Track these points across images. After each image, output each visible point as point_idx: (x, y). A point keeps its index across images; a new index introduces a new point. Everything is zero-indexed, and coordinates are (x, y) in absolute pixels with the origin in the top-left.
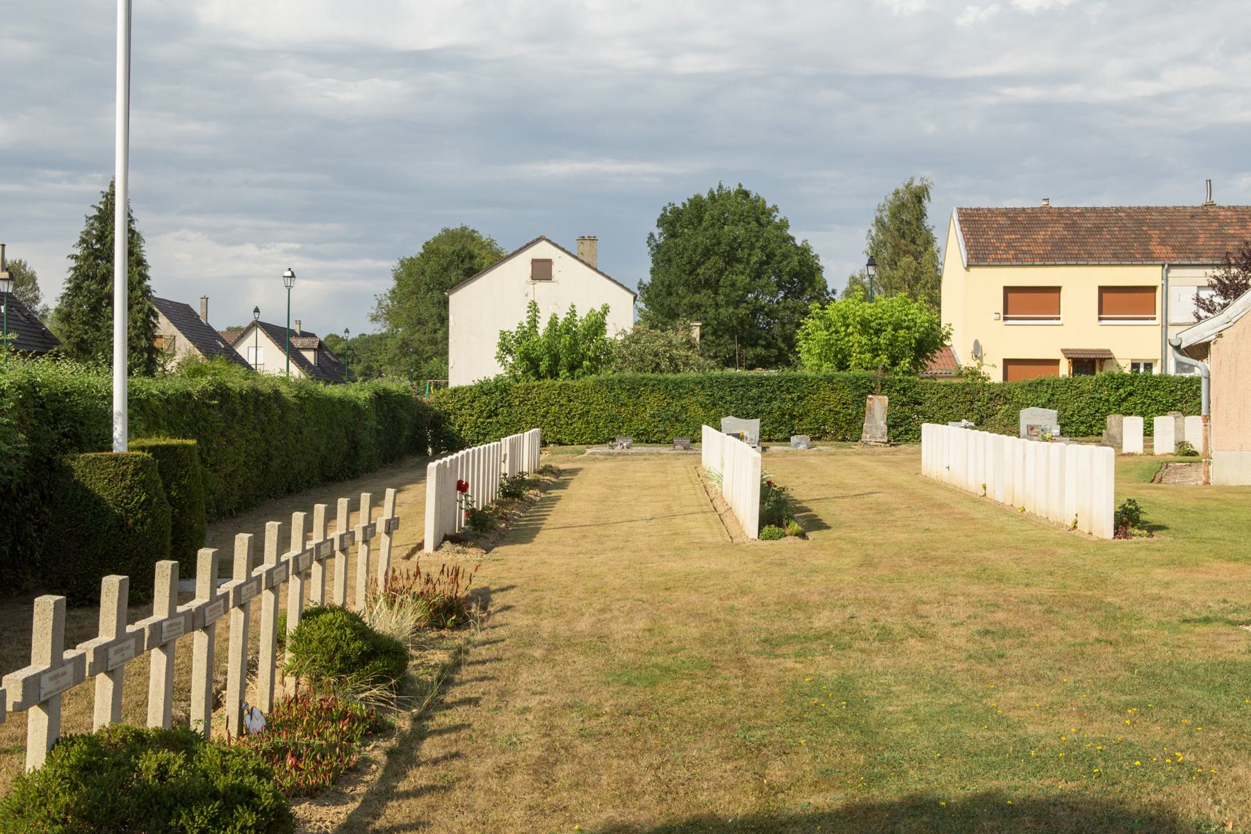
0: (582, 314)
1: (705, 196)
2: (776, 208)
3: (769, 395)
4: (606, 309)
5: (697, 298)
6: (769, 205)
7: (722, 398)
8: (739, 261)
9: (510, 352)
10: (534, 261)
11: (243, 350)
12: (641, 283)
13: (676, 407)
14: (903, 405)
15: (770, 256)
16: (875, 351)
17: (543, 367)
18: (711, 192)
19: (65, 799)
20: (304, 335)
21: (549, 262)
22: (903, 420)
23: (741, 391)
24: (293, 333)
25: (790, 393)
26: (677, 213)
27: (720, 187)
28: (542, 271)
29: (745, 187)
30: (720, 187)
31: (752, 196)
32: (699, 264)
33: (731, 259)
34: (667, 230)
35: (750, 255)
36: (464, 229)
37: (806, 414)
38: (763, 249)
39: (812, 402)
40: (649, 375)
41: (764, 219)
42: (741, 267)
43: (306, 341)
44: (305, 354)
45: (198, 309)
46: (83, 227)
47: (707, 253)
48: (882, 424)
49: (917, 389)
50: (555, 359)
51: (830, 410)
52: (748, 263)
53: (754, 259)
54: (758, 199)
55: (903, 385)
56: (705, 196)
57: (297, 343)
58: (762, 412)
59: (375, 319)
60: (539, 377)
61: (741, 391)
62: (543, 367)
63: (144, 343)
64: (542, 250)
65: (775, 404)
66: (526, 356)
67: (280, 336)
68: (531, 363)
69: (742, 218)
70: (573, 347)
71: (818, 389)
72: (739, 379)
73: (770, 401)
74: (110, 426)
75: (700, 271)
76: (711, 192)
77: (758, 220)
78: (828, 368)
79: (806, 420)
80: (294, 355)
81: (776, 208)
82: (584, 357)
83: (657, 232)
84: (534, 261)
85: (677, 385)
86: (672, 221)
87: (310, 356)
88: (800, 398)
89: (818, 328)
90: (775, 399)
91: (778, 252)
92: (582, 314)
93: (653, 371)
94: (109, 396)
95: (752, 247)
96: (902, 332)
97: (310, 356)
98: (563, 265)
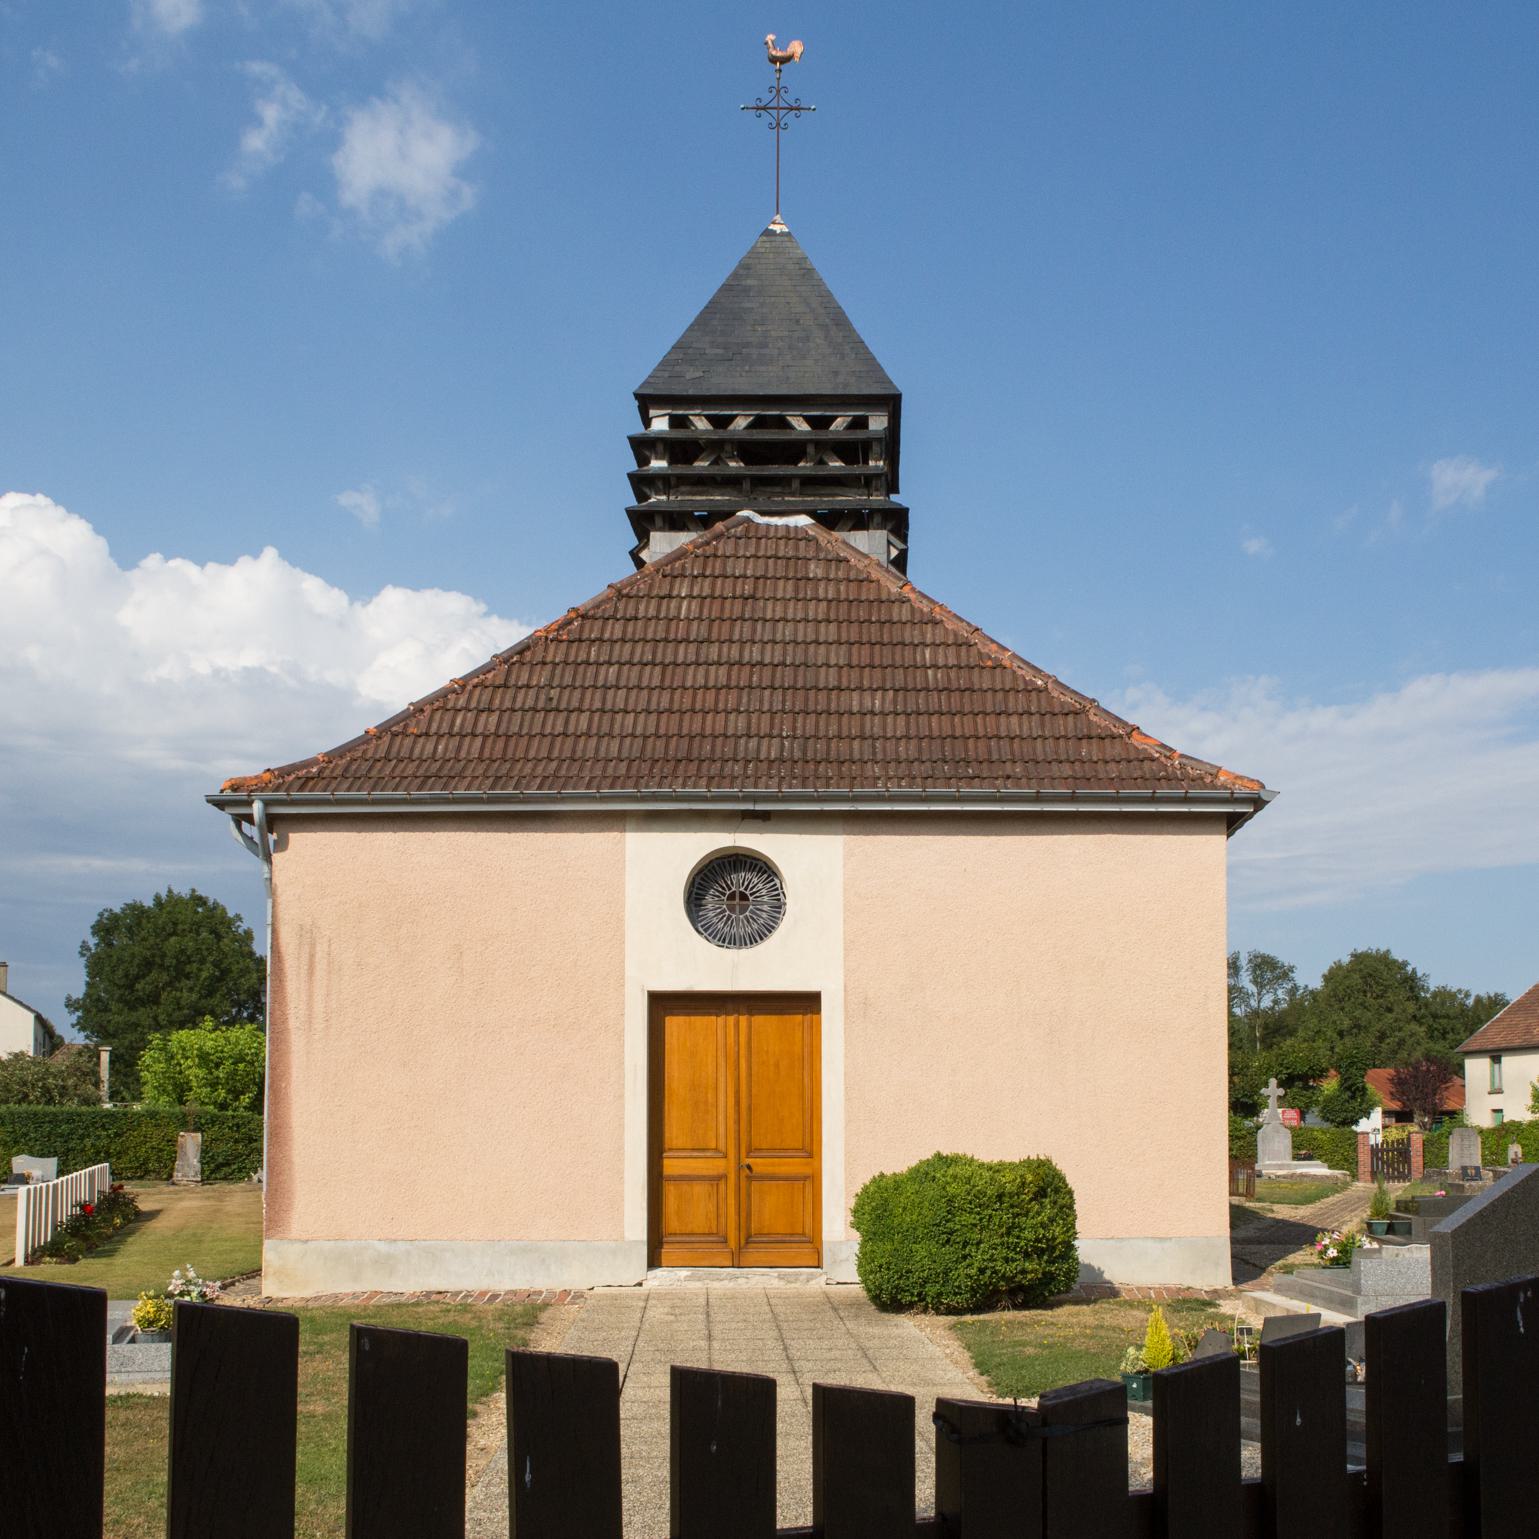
1: (149, 903)
2: (239, 918)
3: (81, 1132)
5: (134, 1017)
6: (231, 914)
7: (25, 1135)
8: (188, 977)
12: (69, 999)
14: (236, 1141)
15: (225, 972)
16: (214, 1085)
18: (157, 898)
19: (1428, 996)
22: (237, 1157)
23: (47, 1128)
25: (106, 1130)
26: (115, 919)
27: (170, 891)
29: (200, 892)
30: (170, 891)
31: (211, 902)
32: (137, 978)
33: (180, 974)
34: (102, 939)
35: (200, 970)
36: (1358, 958)
38: (216, 965)
41: (222, 930)
42: (190, 983)
47: (148, 965)
48: (194, 1161)
49: (252, 1126)
51: (153, 1148)
52: (198, 977)
53: (204, 974)
54: (216, 906)
55: (236, 1121)
56: (149, 903)
58: (73, 1149)
59: (1414, 969)
61: (47, 1128)
65: (88, 1142)
69: (196, 928)
71: (139, 1125)
72: (46, 1115)
73: (82, 1138)
75: (138, 986)
76: (157, 898)
77: (213, 931)
78: (163, 1104)
79: (125, 1159)
81: (239, 918)
83: (92, 941)
86: (107, 927)
88: (117, 1135)
89: (157, 1061)
90: (89, 1136)
91: (234, 968)
93: (19, 1102)
95: (203, 961)
96: (241, 1066)
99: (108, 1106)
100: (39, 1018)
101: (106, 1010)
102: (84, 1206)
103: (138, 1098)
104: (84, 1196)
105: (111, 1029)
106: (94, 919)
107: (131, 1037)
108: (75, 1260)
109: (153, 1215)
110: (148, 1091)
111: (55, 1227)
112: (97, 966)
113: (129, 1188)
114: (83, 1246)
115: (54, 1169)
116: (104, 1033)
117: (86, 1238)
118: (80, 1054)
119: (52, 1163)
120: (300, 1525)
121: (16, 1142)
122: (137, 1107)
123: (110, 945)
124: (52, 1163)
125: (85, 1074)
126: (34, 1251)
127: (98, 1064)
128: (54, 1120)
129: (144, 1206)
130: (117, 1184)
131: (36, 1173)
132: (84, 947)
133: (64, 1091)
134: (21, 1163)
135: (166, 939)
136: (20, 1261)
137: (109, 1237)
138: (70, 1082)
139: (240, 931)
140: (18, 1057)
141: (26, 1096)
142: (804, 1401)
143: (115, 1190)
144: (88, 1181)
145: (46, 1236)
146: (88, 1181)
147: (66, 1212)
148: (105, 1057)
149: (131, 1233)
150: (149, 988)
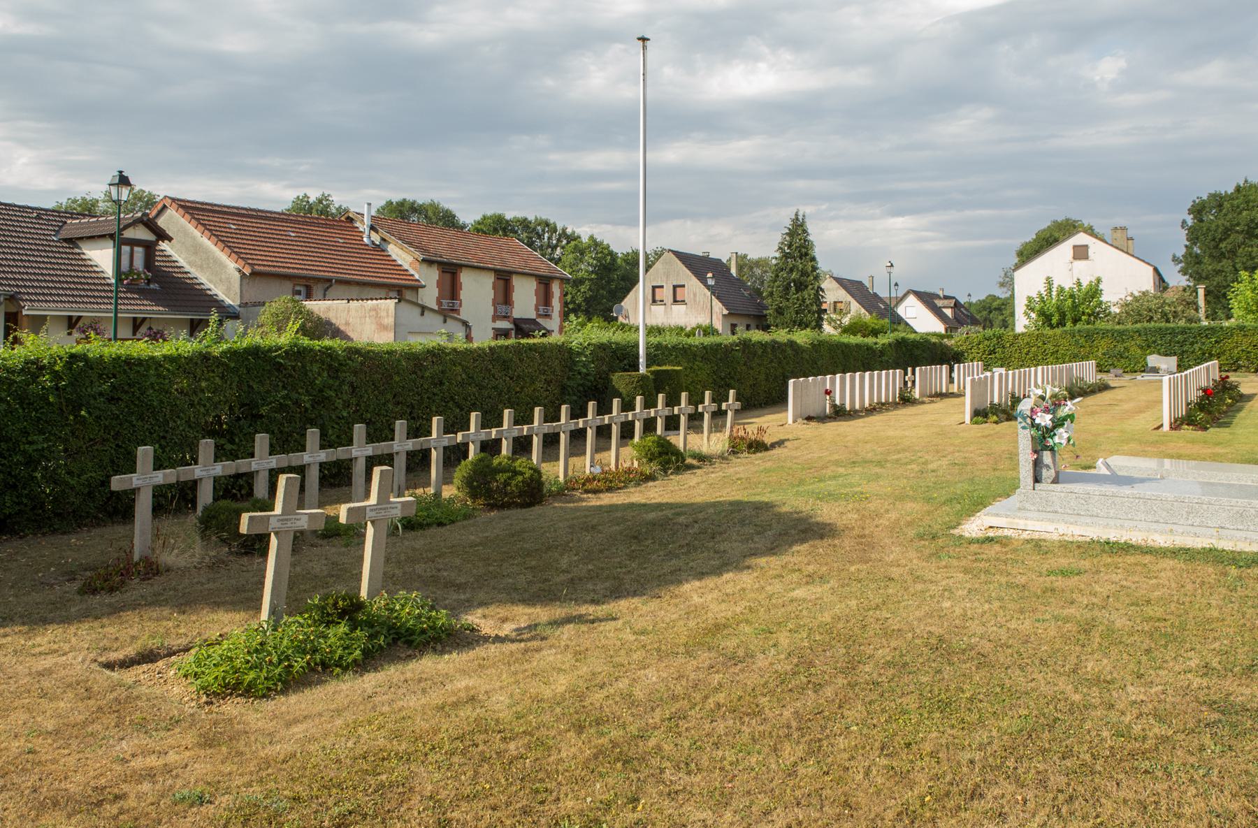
0: (1085, 283)
4: (1099, 280)
7: (1154, 342)
9: (1032, 310)
10: (1075, 247)
11: (901, 311)
13: (1120, 347)
17: (1054, 321)
20: (946, 297)
21: (1086, 246)
23: (1168, 337)
24: (938, 297)
28: (1081, 253)
32: (1221, 240)
36: (1067, 220)
37: (1223, 353)
39: (1228, 344)
40: (1146, 324)
43: (946, 302)
44: (946, 311)
45: (867, 284)
46: (779, 239)
47: (1227, 232)
50: (1063, 315)
57: (939, 303)
60: (1052, 327)
61: (1168, 337)
62: (1054, 321)
63: (815, 308)
64: (1081, 238)
65: (1196, 346)
66: (1042, 313)
67: (928, 299)
68: (1045, 317)
70: (1075, 307)
72: (1167, 329)
73: (1192, 344)
74: (638, 358)
80: (938, 312)
82: (1083, 313)
83: (1190, 220)
84: (1075, 247)
85: (1121, 333)
87: (948, 312)
88: (1216, 342)
92: (1085, 283)
94: (637, 345)
97: (948, 312)
98: (1095, 246)
99: (1205, 323)
100: (1156, 270)
101: (1199, 263)
102: (1205, 390)
103: (1229, 317)
104: (1204, 384)
105: (1204, 275)
106: (1189, 205)
107: (1219, 279)
108: (1206, 429)
109: (1249, 398)
110: (1236, 312)
111: (1188, 404)
112: (1194, 235)
113: (1233, 378)
114: (1209, 418)
115: (1175, 364)
116: (1198, 277)
117: (1210, 413)
118: (1184, 290)
119: (1173, 361)
120: (13, 637)
121: (1149, 347)
122: (1226, 324)
123: (1201, 221)
124: (1173, 361)
125: (1188, 304)
126: (1176, 420)
127: (1197, 297)
128: (1173, 332)
129: (1244, 390)
130: (1224, 375)
131: (1163, 366)
132: (1184, 222)
133: (1175, 315)
134: (1153, 360)
135: (1240, 213)
136: (1166, 427)
137: (1225, 412)
138: (1179, 309)
139: (334, 211)
140: (1144, 294)
141: (1152, 318)
142: (531, 633)
143: (1224, 379)
144: (1205, 373)
145: (1182, 411)
146: (1205, 373)
147: (1194, 395)
148: (1201, 292)
149: (1239, 410)
150: (1229, 247)
